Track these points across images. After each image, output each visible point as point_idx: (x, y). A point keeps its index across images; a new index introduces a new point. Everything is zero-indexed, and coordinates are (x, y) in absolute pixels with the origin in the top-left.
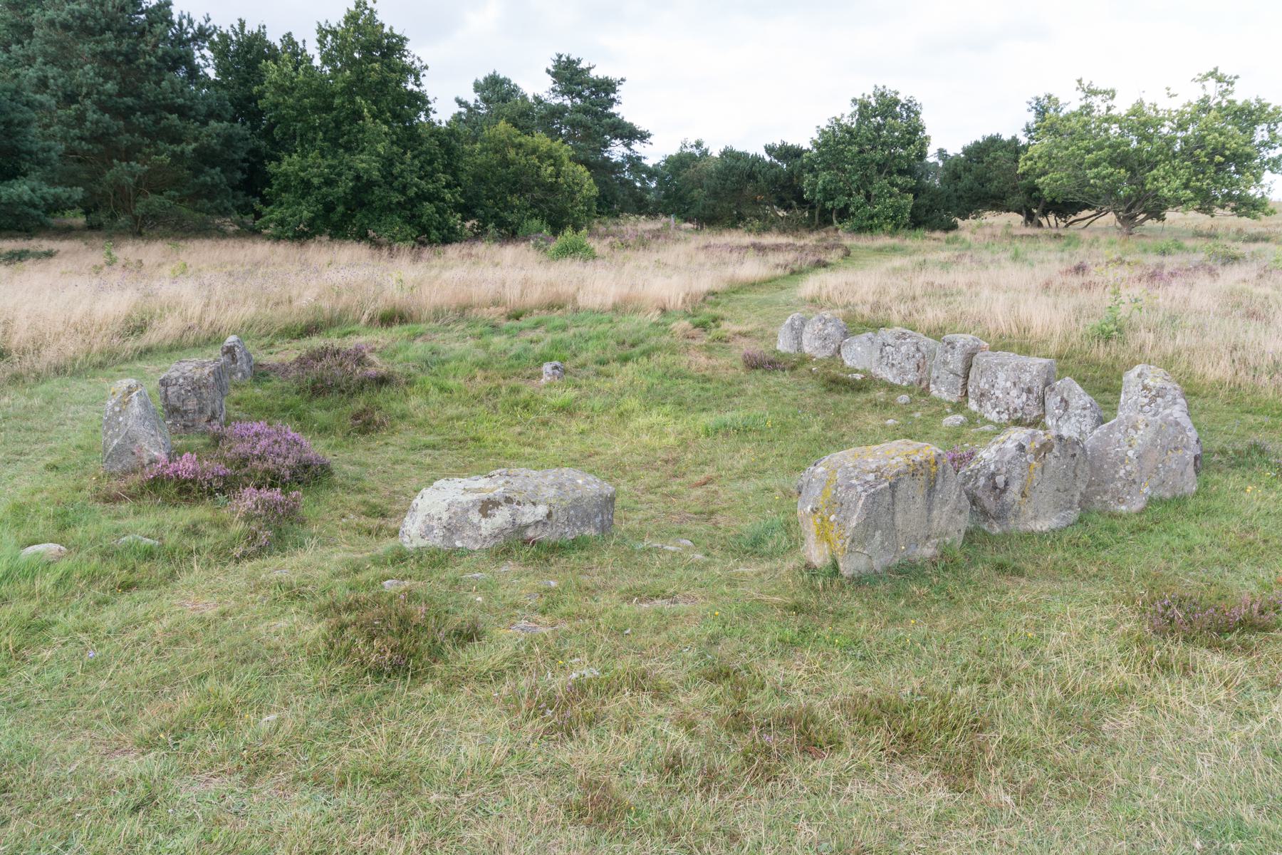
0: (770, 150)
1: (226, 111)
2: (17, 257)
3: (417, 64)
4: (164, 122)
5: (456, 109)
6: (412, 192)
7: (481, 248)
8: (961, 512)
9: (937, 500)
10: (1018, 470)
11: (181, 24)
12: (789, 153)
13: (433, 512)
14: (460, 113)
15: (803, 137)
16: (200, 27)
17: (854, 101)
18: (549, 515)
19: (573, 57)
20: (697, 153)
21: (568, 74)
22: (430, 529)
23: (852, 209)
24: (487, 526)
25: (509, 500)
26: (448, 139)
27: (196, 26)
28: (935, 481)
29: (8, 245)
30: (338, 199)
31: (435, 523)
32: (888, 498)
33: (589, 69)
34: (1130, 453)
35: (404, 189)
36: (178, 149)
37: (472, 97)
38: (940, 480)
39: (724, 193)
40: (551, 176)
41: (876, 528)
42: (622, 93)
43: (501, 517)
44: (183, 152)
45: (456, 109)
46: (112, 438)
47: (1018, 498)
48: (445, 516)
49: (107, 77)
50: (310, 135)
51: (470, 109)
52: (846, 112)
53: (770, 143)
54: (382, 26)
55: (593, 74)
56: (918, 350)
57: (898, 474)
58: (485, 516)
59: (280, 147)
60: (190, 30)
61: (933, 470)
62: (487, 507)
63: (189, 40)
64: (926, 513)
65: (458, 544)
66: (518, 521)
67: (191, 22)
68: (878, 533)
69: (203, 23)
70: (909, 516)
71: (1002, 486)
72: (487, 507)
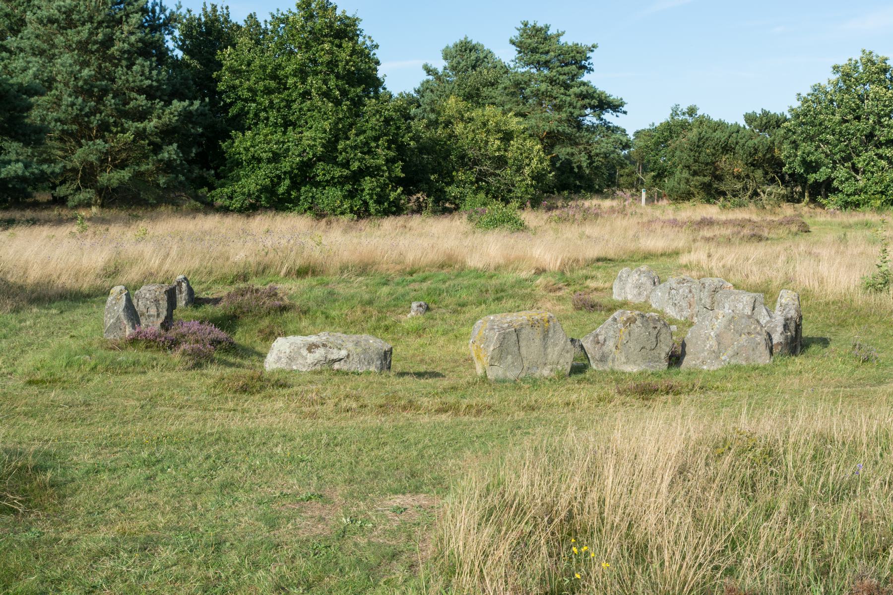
0: (750, 119)
1: (189, 88)
2: (10, 223)
3: (368, 43)
4: (132, 104)
5: (424, 76)
6: (355, 166)
7: (416, 221)
8: (568, 352)
9: (549, 343)
10: (612, 333)
11: (153, 11)
12: (767, 123)
13: (282, 348)
14: (428, 81)
15: (782, 103)
16: (172, 13)
17: (836, 69)
18: (348, 356)
19: (540, 25)
20: (690, 120)
21: (535, 42)
22: (280, 358)
23: (835, 184)
24: (311, 358)
25: (324, 345)
26: (405, 109)
27: (167, 13)
28: (548, 331)
29: (7, 215)
30: (285, 173)
31: (282, 355)
32: (515, 337)
33: (559, 35)
34: (712, 334)
35: (346, 165)
36: (140, 125)
37: (440, 65)
38: (552, 331)
39: (714, 165)
40: (499, 149)
41: (508, 353)
42: (595, 59)
43: (319, 353)
44: (145, 129)
45: (424, 76)
46: (110, 319)
47: (614, 349)
48: (288, 351)
49: (85, 64)
50: (263, 114)
51: (438, 78)
52: (826, 78)
53: (750, 112)
54: (335, 8)
55: (562, 40)
56: (690, 292)
57: (522, 324)
58: (310, 352)
59: (239, 123)
60: (162, 16)
61: (546, 325)
62: (311, 348)
63: (160, 26)
64: (542, 349)
65: (295, 368)
66: (329, 357)
67: (163, 10)
68: (509, 357)
69: (175, 9)
70: (531, 348)
71: (602, 342)
72: (311, 348)
